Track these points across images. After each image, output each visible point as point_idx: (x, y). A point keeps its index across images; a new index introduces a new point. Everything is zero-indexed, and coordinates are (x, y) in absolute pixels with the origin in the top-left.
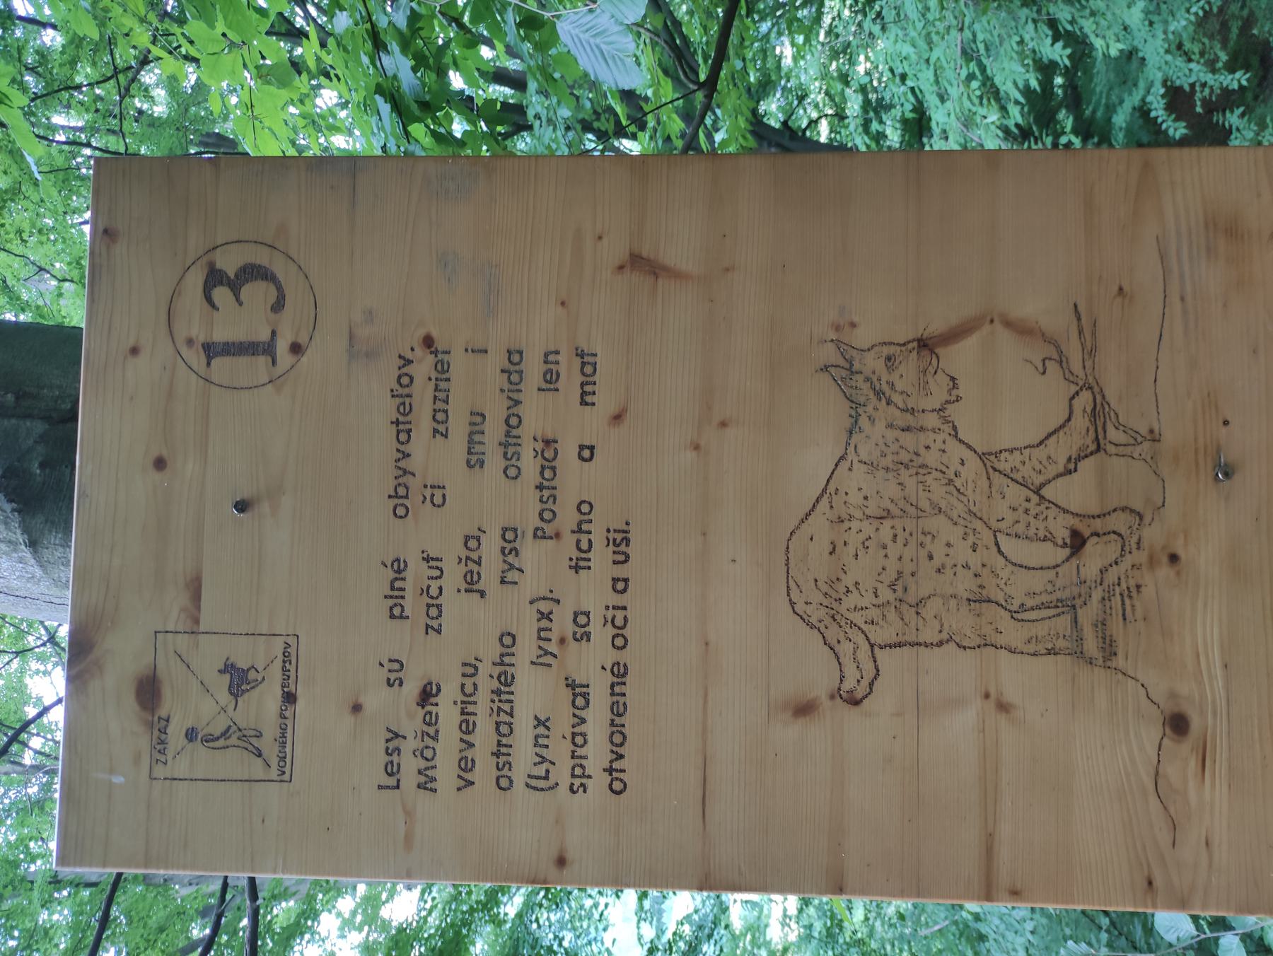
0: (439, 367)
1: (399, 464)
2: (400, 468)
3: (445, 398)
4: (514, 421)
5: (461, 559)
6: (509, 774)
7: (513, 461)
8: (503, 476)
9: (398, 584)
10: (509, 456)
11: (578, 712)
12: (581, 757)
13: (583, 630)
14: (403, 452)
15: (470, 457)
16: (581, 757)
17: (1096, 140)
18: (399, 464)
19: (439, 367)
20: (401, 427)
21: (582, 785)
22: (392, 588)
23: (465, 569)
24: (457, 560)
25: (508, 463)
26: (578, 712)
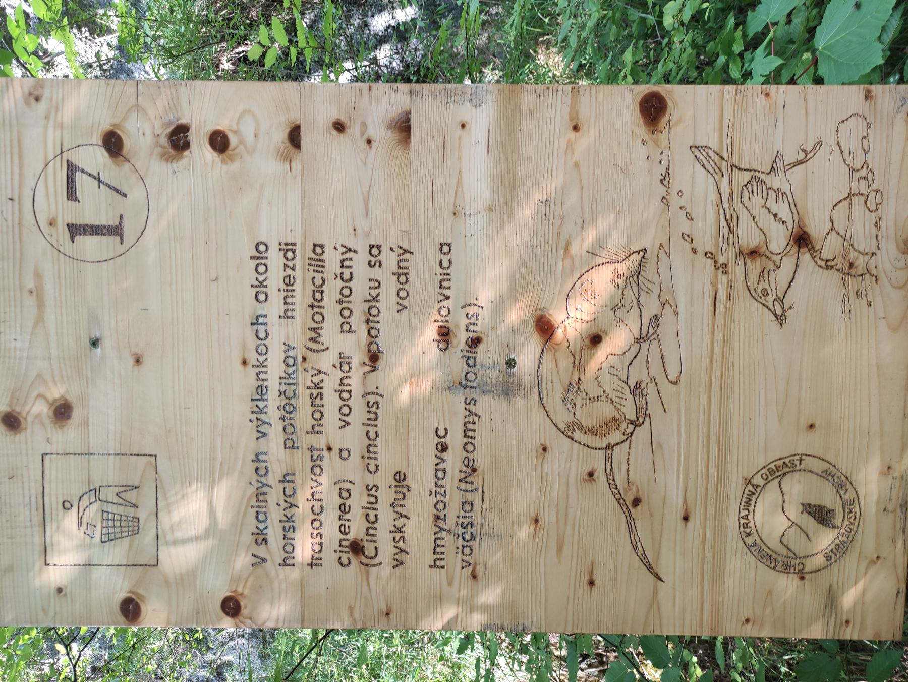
0: (287, 280)
1: (396, 557)
2: (397, 548)
3: (292, 266)
4: (403, 294)
5: (431, 493)
6: (376, 494)
7: (318, 462)
8: (381, 310)
9: (371, 532)
10: (315, 458)
11: (401, 301)
12: (290, 539)
13: (318, 531)
14: (444, 295)
15: (344, 270)
16: (290, 539)
17: (491, 66)
18: (396, 557)
19: (287, 280)
20: (344, 305)
21: (264, 539)
22: (399, 267)
23: (435, 500)
24: (429, 493)
25: (314, 463)
26: (401, 301)
